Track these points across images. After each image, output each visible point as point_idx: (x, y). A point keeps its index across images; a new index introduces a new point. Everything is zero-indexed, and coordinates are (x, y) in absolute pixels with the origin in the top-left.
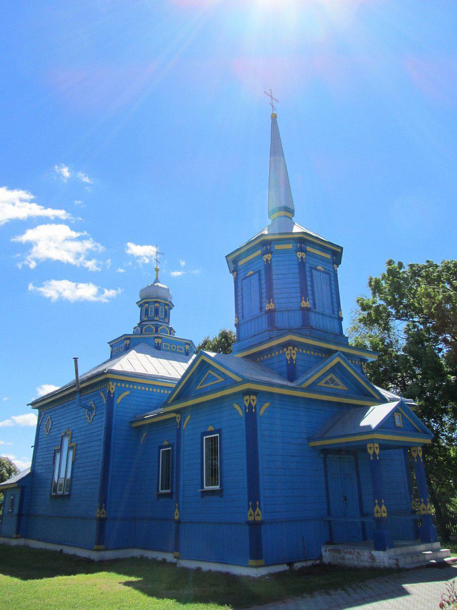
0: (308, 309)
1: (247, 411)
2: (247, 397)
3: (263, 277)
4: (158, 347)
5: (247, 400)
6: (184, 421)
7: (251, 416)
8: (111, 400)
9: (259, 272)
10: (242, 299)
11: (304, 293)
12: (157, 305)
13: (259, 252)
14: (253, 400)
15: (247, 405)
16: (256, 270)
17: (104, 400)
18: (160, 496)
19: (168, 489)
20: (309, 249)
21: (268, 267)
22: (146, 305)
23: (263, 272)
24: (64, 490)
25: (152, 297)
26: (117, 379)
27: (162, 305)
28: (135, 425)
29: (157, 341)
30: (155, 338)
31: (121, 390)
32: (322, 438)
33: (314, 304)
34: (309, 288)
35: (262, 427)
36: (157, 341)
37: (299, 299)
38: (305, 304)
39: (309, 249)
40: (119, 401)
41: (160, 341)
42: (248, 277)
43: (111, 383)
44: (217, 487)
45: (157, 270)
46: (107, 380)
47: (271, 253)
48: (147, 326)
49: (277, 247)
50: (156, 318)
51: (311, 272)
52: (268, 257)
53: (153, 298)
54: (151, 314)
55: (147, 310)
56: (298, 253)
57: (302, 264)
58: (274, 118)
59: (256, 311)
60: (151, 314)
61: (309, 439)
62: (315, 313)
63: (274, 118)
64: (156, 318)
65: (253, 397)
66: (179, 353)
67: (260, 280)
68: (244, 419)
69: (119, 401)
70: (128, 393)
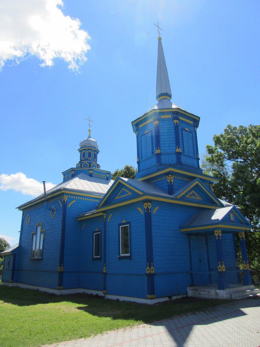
0: (179, 154)
1: (146, 211)
2: (146, 204)
4: (91, 175)
5: (146, 205)
6: (108, 217)
7: (148, 215)
8: (65, 205)
11: (178, 144)
12: (90, 151)
14: (149, 205)
15: (146, 208)
19: (99, 256)
20: (181, 118)
27: (93, 151)
28: (79, 219)
29: (90, 172)
30: (90, 170)
31: (70, 200)
32: (188, 227)
36: (90, 172)
37: (175, 148)
38: (178, 150)
39: (181, 118)
40: (69, 206)
41: (92, 172)
43: (65, 196)
44: (128, 255)
46: (63, 194)
48: (84, 163)
51: (182, 132)
54: (87, 156)
57: (176, 127)
58: (160, 39)
60: (87, 156)
61: (180, 228)
62: (184, 155)
63: (160, 39)
66: (103, 179)
68: (144, 215)
69: (69, 206)
70: (74, 201)
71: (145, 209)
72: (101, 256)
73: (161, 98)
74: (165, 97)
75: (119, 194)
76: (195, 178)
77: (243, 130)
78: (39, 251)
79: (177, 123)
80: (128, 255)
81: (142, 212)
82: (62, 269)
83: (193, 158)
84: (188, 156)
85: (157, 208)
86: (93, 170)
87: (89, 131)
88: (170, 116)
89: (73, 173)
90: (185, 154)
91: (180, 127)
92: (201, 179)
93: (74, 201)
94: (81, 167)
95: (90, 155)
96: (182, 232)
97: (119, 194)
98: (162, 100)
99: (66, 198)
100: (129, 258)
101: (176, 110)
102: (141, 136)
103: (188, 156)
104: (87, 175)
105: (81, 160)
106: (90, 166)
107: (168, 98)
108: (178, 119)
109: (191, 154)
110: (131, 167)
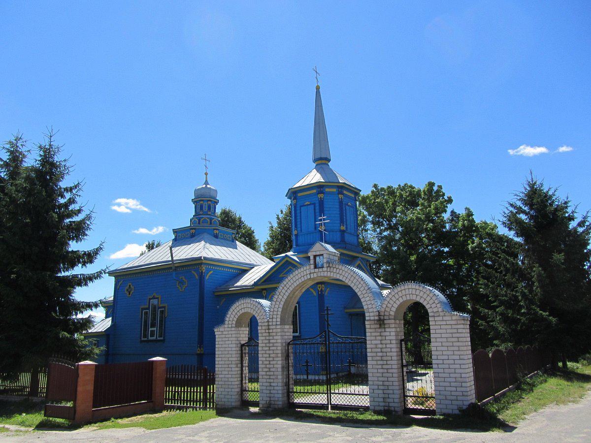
0: (343, 231)
2: (319, 286)
3: (317, 208)
4: (216, 236)
5: (319, 287)
7: (321, 296)
8: (202, 276)
9: (314, 204)
10: (301, 219)
11: (342, 221)
12: (209, 202)
13: (315, 191)
16: (313, 202)
17: (196, 275)
18: (142, 341)
19: (162, 337)
20: (345, 192)
21: (321, 202)
22: (202, 202)
23: (317, 205)
24: (157, 335)
25: (206, 196)
26: (219, 265)
28: (216, 294)
29: (216, 232)
30: (214, 229)
31: (208, 270)
32: (353, 308)
33: (347, 228)
34: (344, 217)
35: (328, 303)
36: (216, 232)
37: (339, 225)
38: (343, 228)
39: (345, 192)
40: (207, 278)
41: (217, 232)
42: (305, 205)
43: (203, 266)
44: (162, 338)
45: (206, 174)
46: (201, 264)
47: (324, 193)
49: (327, 190)
50: (209, 213)
51: (345, 207)
52: (322, 196)
53: (207, 198)
54: (205, 209)
55: (202, 206)
56: (340, 195)
57: (341, 202)
58: (318, 88)
59: (312, 229)
60: (205, 209)
61: (345, 308)
62: (347, 233)
63: (318, 88)
64: (209, 213)
65: (323, 286)
66: (228, 240)
67: (315, 209)
68: (317, 297)
69: (207, 278)
70: (212, 272)
71: (318, 291)
72: (164, 337)
73: (320, 162)
74: (323, 162)
75: (284, 272)
76: (356, 258)
77: (391, 192)
78: (157, 331)
79: (341, 198)
80: (162, 338)
81: (315, 294)
82: (202, 351)
83: (353, 235)
84: (350, 234)
85: (328, 289)
86: (218, 230)
87: (206, 174)
88: (334, 190)
89: (193, 232)
90: (349, 231)
91: (344, 203)
92: (362, 258)
93: (212, 272)
94: (199, 223)
95: (209, 207)
96: (346, 312)
97: (284, 272)
98: (322, 166)
99: (204, 268)
100: (163, 341)
101: (342, 185)
102: (301, 207)
103: (350, 234)
104: (212, 235)
105: (197, 214)
106: (211, 223)
107: (327, 162)
108: (342, 194)
109: (353, 231)
110: (230, 211)
